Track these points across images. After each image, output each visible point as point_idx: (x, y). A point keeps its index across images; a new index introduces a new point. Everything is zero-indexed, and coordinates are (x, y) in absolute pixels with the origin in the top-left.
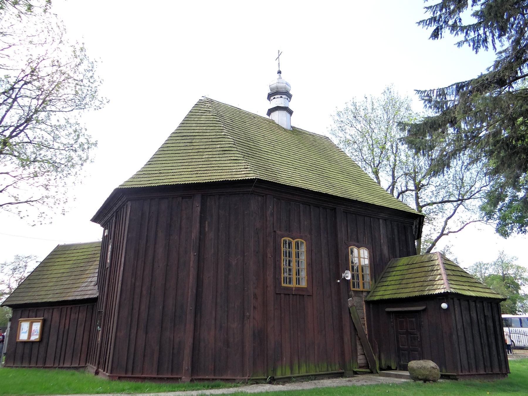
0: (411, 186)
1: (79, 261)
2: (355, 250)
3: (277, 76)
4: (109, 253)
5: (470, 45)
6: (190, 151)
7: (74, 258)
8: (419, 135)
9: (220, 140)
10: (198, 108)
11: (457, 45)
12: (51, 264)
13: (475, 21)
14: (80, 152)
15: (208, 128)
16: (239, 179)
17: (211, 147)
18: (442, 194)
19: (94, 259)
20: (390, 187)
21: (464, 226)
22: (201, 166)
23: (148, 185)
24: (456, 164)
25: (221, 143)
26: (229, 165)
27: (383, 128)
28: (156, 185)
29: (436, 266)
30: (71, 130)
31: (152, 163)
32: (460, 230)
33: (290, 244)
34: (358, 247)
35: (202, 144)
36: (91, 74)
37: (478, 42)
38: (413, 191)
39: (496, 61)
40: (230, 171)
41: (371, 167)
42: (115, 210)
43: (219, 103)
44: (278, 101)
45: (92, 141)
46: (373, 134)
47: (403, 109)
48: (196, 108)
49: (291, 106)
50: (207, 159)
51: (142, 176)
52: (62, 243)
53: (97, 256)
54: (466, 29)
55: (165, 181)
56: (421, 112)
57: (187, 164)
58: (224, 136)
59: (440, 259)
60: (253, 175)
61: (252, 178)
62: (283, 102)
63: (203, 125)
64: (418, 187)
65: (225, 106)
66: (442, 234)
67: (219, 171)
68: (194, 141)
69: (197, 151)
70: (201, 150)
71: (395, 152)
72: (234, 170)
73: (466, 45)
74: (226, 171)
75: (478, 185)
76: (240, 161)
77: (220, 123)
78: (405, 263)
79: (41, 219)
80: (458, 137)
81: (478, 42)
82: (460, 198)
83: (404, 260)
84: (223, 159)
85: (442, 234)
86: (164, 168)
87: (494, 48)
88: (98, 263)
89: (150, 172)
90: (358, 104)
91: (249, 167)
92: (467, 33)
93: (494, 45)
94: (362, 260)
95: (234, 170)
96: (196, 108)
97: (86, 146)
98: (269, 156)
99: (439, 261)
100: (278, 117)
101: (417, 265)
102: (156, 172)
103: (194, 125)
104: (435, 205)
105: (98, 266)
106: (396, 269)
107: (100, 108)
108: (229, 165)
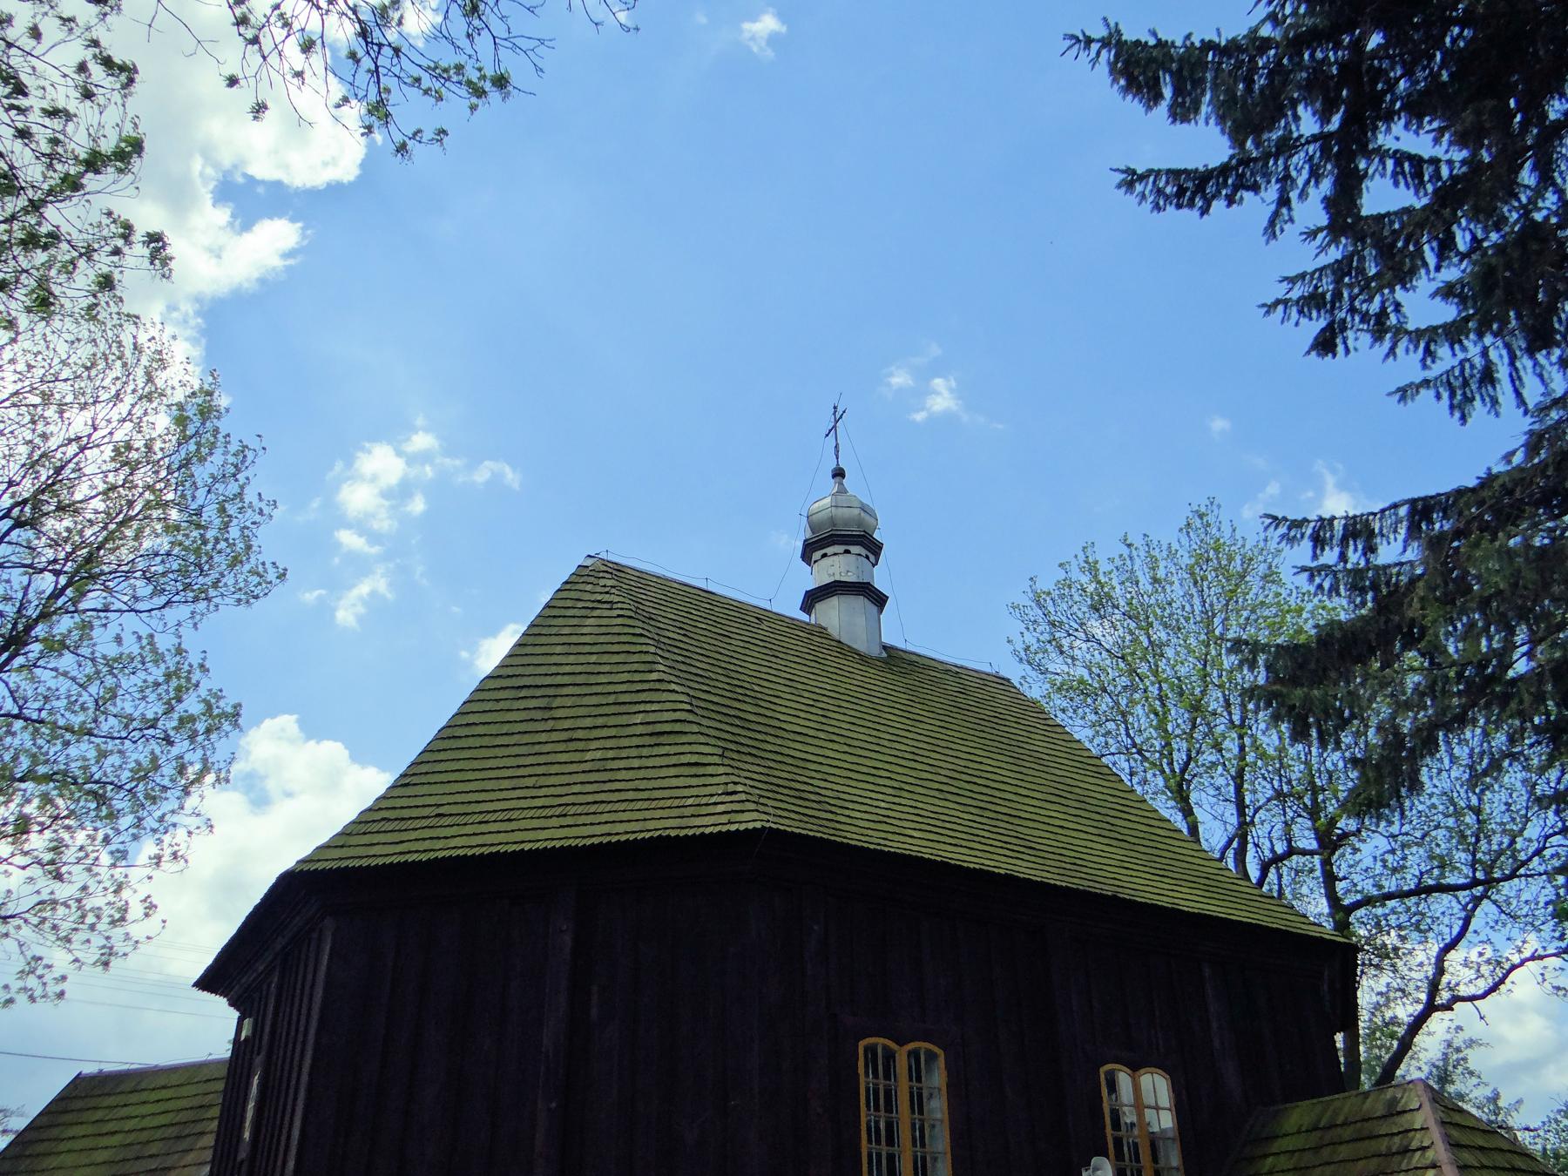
0: (1307, 841)
1: (144, 1136)
2: (1124, 1079)
3: (832, 485)
4: (251, 1105)
5: (1438, 397)
6: (543, 737)
7: (130, 1125)
8: (1307, 680)
9: (642, 697)
10: (573, 595)
11: (1397, 396)
12: (40, 1148)
13: (1447, 312)
14: (181, 746)
15: (605, 658)
16: (707, 831)
17: (612, 721)
18: (1416, 861)
19: (199, 1128)
20: (1230, 842)
21: (1506, 976)
22: (576, 789)
23: (395, 859)
24: (1442, 776)
25: (648, 707)
26: (675, 782)
27: (1192, 641)
28: (424, 857)
29: (1418, 1135)
30: (158, 673)
31: (415, 780)
32: (1494, 988)
33: (890, 1056)
34: (1135, 1067)
35: (582, 712)
36: (233, 488)
37: (1466, 384)
38: (1312, 853)
39: (1531, 433)
40: (676, 803)
41: (1163, 772)
42: (278, 947)
43: (642, 576)
44: (838, 566)
45: (226, 706)
46: (1162, 664)
47: (1254, 581)
48: (564, 595)
49: (880, 579)
50: (598, 765)
51: (376, 827)
52: (90, 1069)
53: (209, 1115)
54: (1428, 339)
55: (453, 842)
56: (1305, 604)
57: (530, 782)
58: (657, 686)
59: (1427, 1107)
60: (755, 815)
61: (751, 826)
62: (853, 569)
63: (587, 649)
64: (1329, 842)
65: (663, 583)
66: (1430, 1008)
67: (639, 805)
68: (557, 702)
69: (565, 736)
70: (580, 734)
71: (1236, 718)
72: (690, 801)
73: (1427, 395)
74: (662, 804)
75: (1533, 831)
76: (710, 770)
77: (643, 640)
78: (1307, 1121)
79: (32, 982)
80: (1434, 683)
81: (1466, 384)
82: (1480, 875)
83: (1300, 1115)
84: (651, 762)
85: (1430, 1008)
86: (451, 799)
87: (1521, 400)
88: (209, 1140)
89: (406, 813)
90: (1104, 566)
91: (740, 788)
92: (1427, 351)
93: (1518, 394)
94: (1149, 1114)
95: (690, 801)
96: (564, 595)
97: (201, 727)
98: (811, 749)
99: (1425, 1117)
100: (834, 616)
101: (1347, 1133)
102: (426, 812)
103: (558, 649)
104: (1391, 904)
105: (208, 1155)
106: (1276, 1146)
107: (256, 597)
108: (675, 782)
